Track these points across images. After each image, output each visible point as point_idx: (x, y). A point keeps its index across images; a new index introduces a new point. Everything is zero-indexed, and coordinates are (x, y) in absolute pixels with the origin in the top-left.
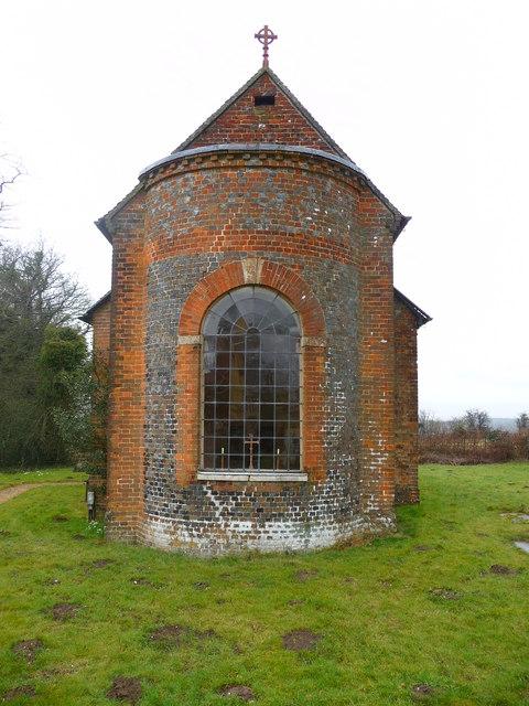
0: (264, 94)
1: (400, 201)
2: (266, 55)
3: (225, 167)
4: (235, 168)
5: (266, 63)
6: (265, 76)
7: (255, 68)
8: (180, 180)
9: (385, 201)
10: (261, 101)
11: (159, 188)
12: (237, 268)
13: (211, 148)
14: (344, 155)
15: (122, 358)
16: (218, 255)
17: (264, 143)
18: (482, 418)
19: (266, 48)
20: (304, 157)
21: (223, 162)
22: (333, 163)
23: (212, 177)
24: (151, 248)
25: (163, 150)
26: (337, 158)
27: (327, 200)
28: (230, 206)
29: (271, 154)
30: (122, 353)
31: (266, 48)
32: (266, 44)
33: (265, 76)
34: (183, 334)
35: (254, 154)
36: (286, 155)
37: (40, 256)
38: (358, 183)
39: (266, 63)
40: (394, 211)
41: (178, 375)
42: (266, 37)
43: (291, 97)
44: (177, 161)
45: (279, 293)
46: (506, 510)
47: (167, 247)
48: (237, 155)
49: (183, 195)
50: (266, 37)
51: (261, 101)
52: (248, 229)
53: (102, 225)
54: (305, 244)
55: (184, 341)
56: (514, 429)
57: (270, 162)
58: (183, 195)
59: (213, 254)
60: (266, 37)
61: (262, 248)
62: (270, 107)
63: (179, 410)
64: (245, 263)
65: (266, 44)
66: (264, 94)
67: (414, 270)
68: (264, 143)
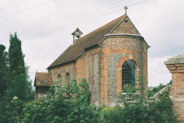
0: (126, 19)
1: (149, 44)
4: (127, 38)
8: (116, 39)
10: (126, 21)
12: (128, 56)
13: (124, 34)
15: (102, 72)
16: (125, 54)
19: (126, 11)
21: (126, 37)
28: (126, 45)
30: (102, 71)
31: (126, 11)
35: (131, 36)
47: (113, 51)
48: (129, 36)
49: (117, 42)
50: (126, 8)
53: (37, 73)
58: (117, 42)
60: (126, 8)
65: (126, 10)
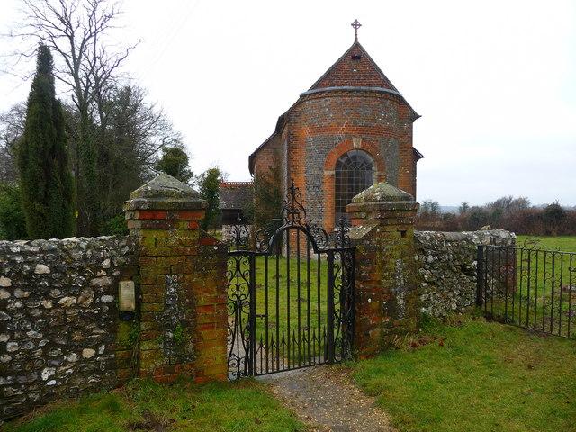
0: (356, 55)
1: (416, 106)
5: (356, 39)
6: (357, 46)
7: (351, 43)
9: (411, 108)
10: (354, 58)
12: (351, 142)
14: (396, 90)
17: (355, 76)
18: (434, 206)
20: (379, 92)
22: (394, 95)
23: (339, 100)
27: (387, 110)
29: (366, 91)
33: (357, 46)
34: (327, 170)
35: (358, 91)
36: (371, 92)
37: (128, 89)
38: (400, 100)
39: (356, 39)
40: (414, 113)
41: (325, 187)
42: (356, 25)
43: (369, 57)
44: (310, 95)
45: (368, 153)
47: (315, 130)
50: (356, 25)
51: (354, 58)
52: (355, 125)
54: (378, 130)
55: (326, 173)
56: (457, 213)
57: (365, 95)
59: (340, 134)
60: (356, 25)
61: (361, 133)
63: (325, 202)
64: (354, 140)
66: (356, 55)
67: (421, 137)
68: (355, 76)
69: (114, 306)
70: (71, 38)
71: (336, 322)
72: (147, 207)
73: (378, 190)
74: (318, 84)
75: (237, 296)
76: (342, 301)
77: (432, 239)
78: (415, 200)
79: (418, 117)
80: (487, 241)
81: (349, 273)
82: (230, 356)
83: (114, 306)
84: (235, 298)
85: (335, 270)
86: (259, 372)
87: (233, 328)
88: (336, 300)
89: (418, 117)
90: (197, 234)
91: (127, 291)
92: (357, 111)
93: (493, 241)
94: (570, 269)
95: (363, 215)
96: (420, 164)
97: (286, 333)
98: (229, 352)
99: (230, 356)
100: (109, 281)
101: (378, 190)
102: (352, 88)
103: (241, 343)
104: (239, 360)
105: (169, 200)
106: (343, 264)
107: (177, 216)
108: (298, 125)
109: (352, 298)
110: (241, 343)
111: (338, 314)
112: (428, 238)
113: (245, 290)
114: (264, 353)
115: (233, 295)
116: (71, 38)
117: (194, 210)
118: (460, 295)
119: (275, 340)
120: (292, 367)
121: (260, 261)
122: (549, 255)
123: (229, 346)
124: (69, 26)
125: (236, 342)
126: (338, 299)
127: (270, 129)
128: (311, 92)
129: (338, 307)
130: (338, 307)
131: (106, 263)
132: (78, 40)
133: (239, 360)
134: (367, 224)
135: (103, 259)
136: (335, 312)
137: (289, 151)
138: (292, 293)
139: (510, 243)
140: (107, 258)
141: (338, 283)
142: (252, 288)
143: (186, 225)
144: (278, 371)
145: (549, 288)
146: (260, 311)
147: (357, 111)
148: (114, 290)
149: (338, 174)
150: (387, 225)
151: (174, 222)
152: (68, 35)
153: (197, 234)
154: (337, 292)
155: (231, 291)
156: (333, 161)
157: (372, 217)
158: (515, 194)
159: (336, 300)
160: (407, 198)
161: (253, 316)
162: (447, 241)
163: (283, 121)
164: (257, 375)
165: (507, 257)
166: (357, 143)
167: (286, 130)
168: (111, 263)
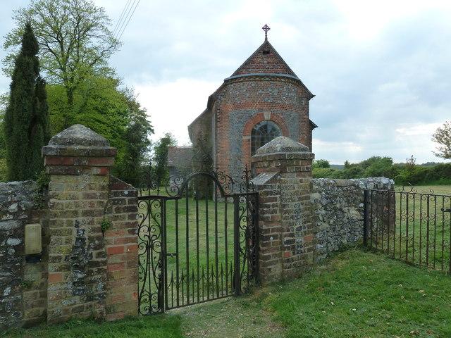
0: (267, 50)
2: (266, 36)
3: (258, 81)
5: (266, 39)
7: (262, 42)
11: (375, 226)
17: (266, 66)
19: (266, 33)
20: (283, 77)
21: (257, 79)
22: (294, 80)
24: (230, 105)
25: (228, 75)
26: (293, 77)
31: (266, 33)
32: (266, 31)
35: (268, 77)
38: (298, 83)
39: (266, 39)
40: (309, 93)
43: (276, 52)
44: (232, 79)
46: (414, 215)
50: (266, 28)
51: (265, 53)
55: (244, 138)
60: (266, 28)
62: (268, 55)
64: (265, 113)
65: (266, 31)
66: (267, 50)
68: (266, 66)
69: (20, 248)
70: (61, 43)
71: (242, 258)
72: (54, 153)
73: (279, 143)
74: (237, 72)
75: (149, 237)
76: (247, 239)
77: (325, 184)
78: (311, 151)
79: (313, 96)
80: (371, 186)
81: (252, 215)
82: (142, 292)
83: (20, 248)
84: (147, 239)
85: (241, 212)
86: (170, 306)
87: (144, 266)
88: (242, 239)
89: (313, 96)
90: (106, 179)
91: (33, 233)
92: (265, 90)
93: (376, 186)
94: (442, 210)
95: (266, 164)
96: (314, 132)
97: (195, 270)
98: (141, 288)
99: (142, 292)
100: (15, 224)
101: (279, 143)
102: (264, 74)
103: (152, 281)
104: (150, 297)
105: (78, 147)
106: (248, 206)
107: (85, 162)
108: (223, 103)
109: (255, 235)
110: (152, 281)
111: (244, 251)
112: (322, 184)
113: (156, 231)
114: (175, 291)
115: (145, 235)
116: (61, 43)
117: (102, 156)
118: (349, 232)
119: (196, 273)
120: (201, 300)
121: (170, 205)
122: (424, 197)
123: (141, 284)
124: (59, 34)
125: (147, 279)
126: (244, 238)
127: (203, 107)
128: (234, 77)
129: (243, 245)
130: (243, 245)
131: (13, 207)
132: (67, 41)
133: (150, 297)
134: (271, 171)
135: (10, 203)
136: (241, 250)
137: (217, 121)
138: (206, 234)
139: (389, 187)
140: (15, 202)
141: (243, 223)
142: (163, 229)
143: (99, 171)
144: (178, 306)
145: (424, 227)
146: (171, 247)
147: (265, 90)
148: (19, 233)
149: (253, 139)
150: (286, 172)
151: (86, 168)
152: (59, 41)
153: (106, 179)
154: (242, 231)
155: (143, 232)
156: (250, 130)
157: (273, 166)
158: (382, 154)
159: (242, 239)
160: (303, 150)
161: (164, 254)
162: (338, 187)
163: (212, 100)
164: (168, 308)
165: (389, 200)
166: (267, 116)
167: (214, 107)
168: (19, 207)
